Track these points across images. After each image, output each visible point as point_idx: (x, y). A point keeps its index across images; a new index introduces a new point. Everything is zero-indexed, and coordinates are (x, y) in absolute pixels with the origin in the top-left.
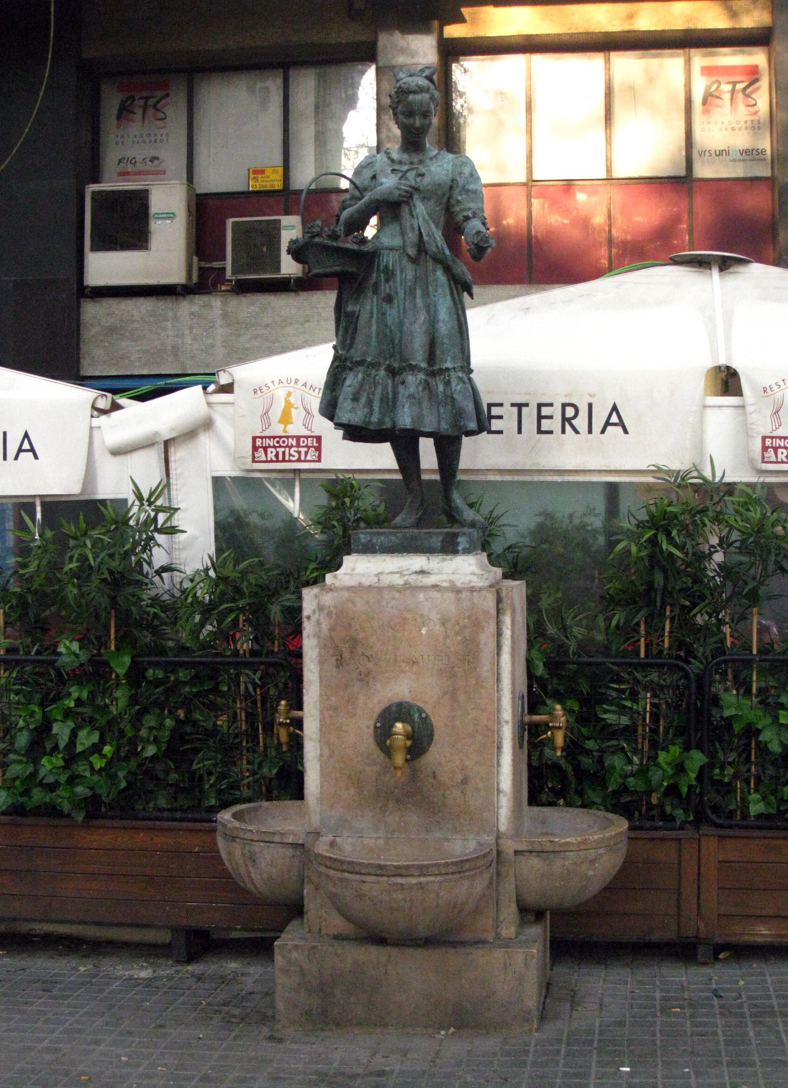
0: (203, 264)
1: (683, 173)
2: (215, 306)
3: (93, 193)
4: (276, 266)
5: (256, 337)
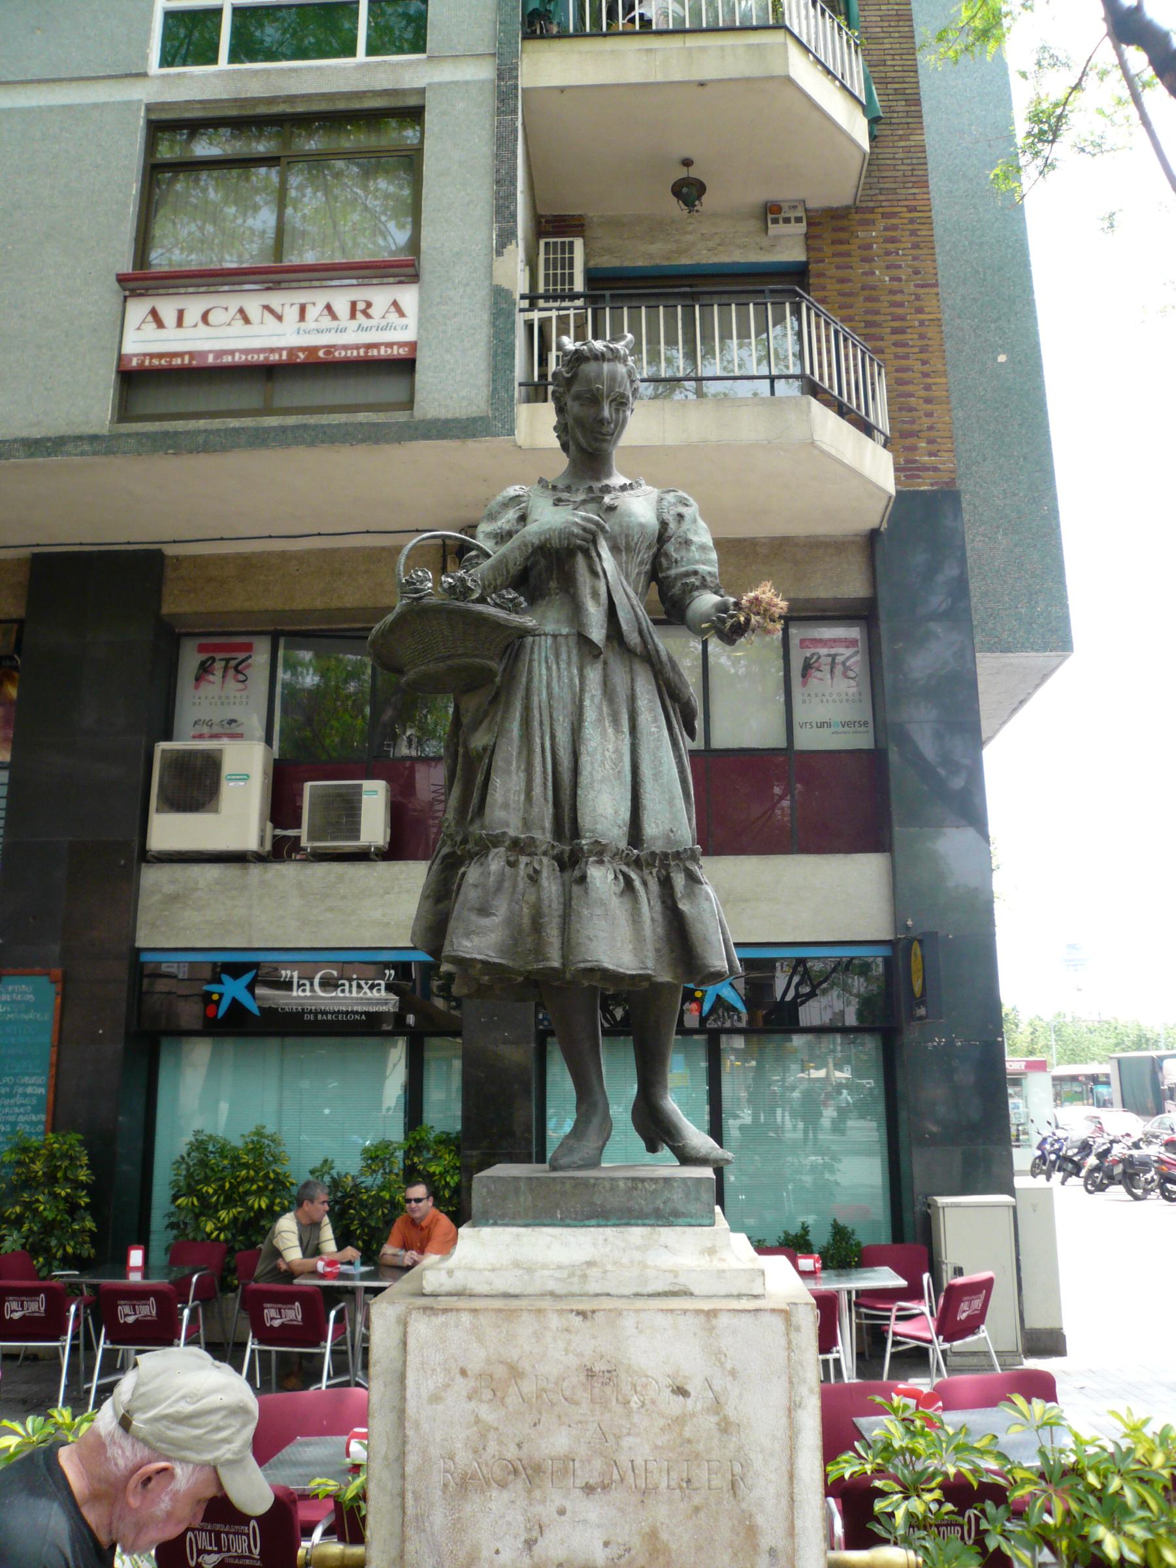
0: (279, 832)
2: (287, 872)
3: (163, 751)
5: (331, 909)
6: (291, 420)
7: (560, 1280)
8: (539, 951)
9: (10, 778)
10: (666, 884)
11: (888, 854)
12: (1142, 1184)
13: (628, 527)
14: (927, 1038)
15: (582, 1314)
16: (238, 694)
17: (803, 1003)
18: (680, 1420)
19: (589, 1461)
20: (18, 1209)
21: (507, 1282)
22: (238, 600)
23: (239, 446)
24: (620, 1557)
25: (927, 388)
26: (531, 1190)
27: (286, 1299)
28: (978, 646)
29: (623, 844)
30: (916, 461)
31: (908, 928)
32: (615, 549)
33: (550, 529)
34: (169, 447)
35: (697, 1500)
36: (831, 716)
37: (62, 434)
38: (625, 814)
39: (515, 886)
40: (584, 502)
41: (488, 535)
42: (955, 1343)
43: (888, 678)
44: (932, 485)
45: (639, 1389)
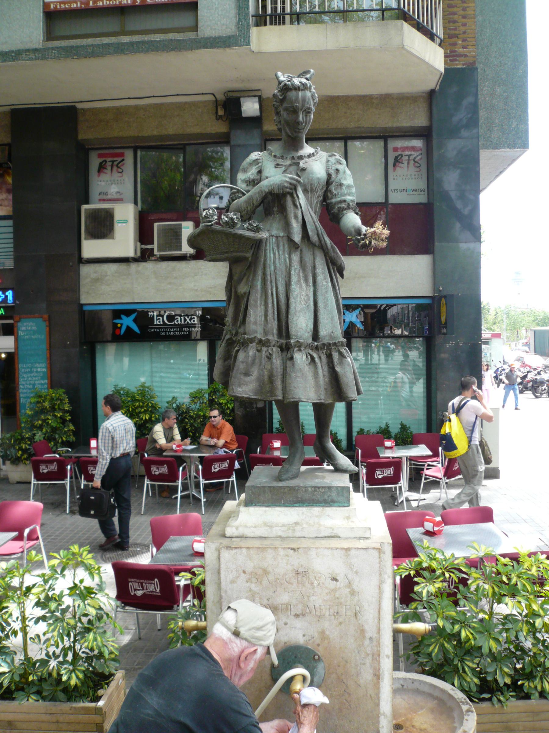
0: (143, 246)
1: (384, 201)
2: (149, 267)
3: (86, 209)
4: (179, 248)
5: (170, 284)
6: (136, 38)
7: (283, 531)
8: (272, 391)
9: (14, 223)
10: (330, 357)
11: (432, 255)
12: (540, 391)
13: (312, 180)
14: (447, 347)
15: (294, 549)
16: (119, 179)
17: (389, 309)
18: (334, 590)
19: (297, 606)
20: (40, 422)
21: (262, 532)
22: (117, 131)
23: (110, 54)
24: (309, 640)
25: (464, 9)
26: (271, 491)
27: (160, 463)
28: (481, 146)
29: (310, 341)
30: (456, 51)
31: (440, 291)
32: (305, 191)
33: (273, 184)
34: (75, 55)
35: (341, 620)
36: (407, 187)
37: (19, 48)
38: (311, 326)
39: (261, 362)
40: (290, 165)
41: (243, 181)
42: (452, 479)
43: (435, 154)
44: (463, 65)
45: (317, 578)
